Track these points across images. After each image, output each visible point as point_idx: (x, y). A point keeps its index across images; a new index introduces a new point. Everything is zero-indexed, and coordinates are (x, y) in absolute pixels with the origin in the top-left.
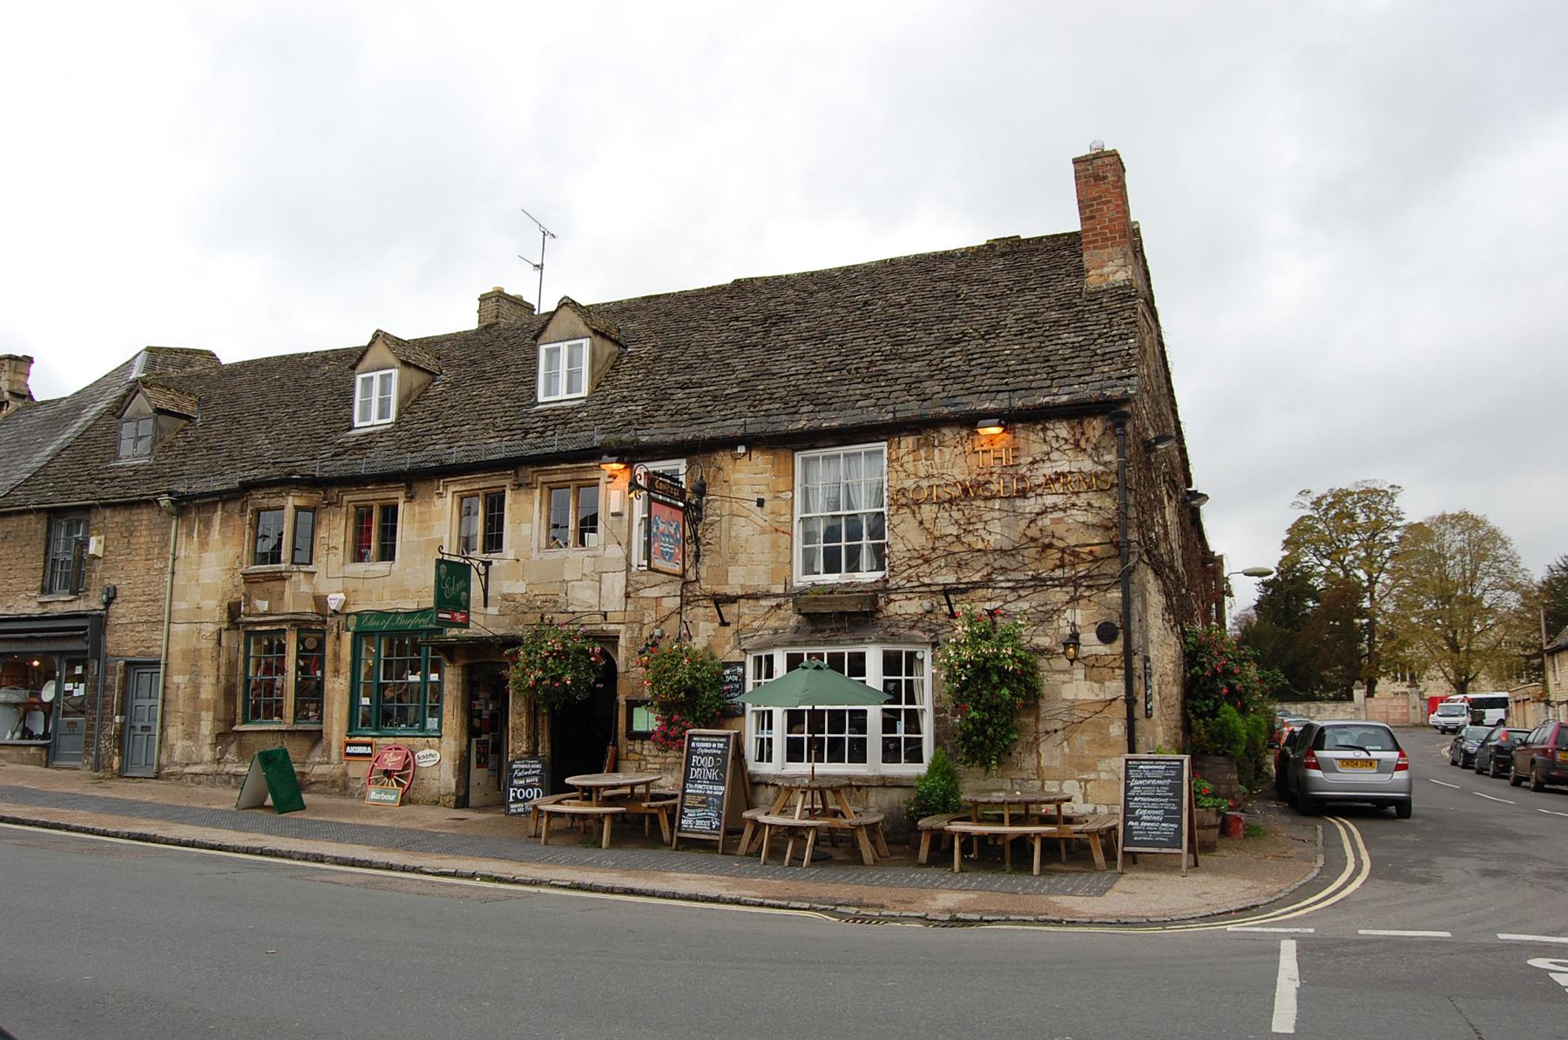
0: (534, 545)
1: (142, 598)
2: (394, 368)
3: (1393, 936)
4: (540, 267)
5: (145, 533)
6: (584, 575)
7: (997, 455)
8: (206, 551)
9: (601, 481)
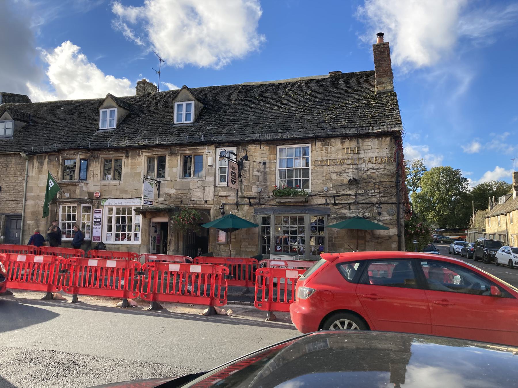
0: (178, 175)
1: (13, 191)
2: (115, 108)
3: (100, 296)
4: (159, 73)
5: (13, 166)
6: (198, 187)
7: (352, 149)
8: (41, 174)
9: (204, 154)
